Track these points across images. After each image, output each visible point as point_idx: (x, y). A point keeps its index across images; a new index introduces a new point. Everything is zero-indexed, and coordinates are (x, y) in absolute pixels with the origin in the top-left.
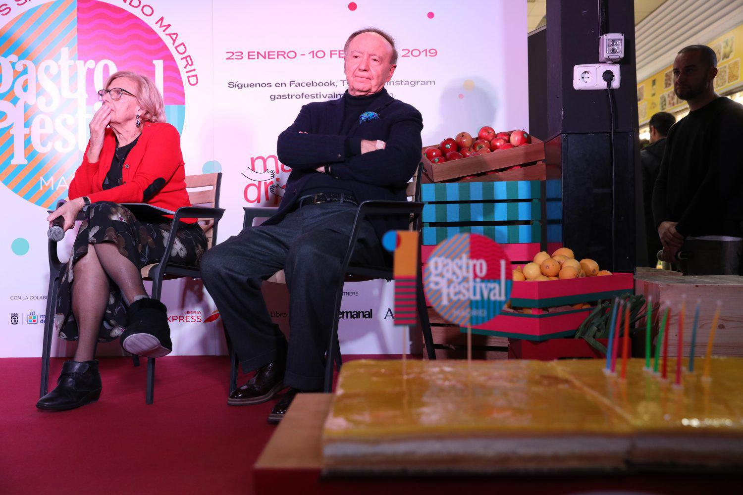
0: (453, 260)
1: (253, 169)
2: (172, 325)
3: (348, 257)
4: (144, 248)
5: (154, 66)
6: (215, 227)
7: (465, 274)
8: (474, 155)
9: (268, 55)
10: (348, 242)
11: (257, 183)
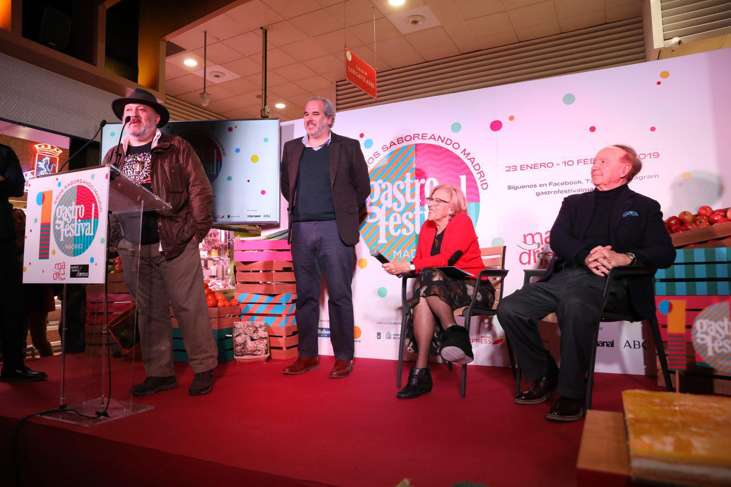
0: (716, 321)
1: (525, 243)
2: (473, 344)
3: (603, 304)
4: (455, 295)
5: (460, 179)
6: (502, 281)
7: (409, 200)
8: (696, 228)
9: (534, 167)
10: (603, 295)
11: (528, 251)
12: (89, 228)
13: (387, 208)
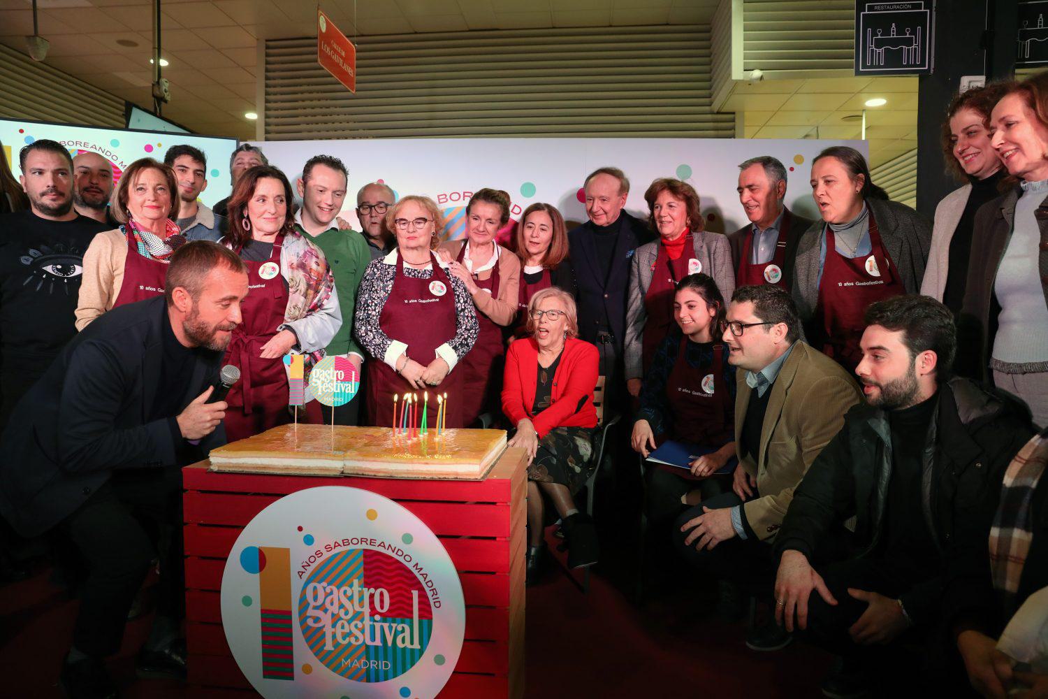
7: (358, 609)
12: (407, 634)
13: (333, 615)
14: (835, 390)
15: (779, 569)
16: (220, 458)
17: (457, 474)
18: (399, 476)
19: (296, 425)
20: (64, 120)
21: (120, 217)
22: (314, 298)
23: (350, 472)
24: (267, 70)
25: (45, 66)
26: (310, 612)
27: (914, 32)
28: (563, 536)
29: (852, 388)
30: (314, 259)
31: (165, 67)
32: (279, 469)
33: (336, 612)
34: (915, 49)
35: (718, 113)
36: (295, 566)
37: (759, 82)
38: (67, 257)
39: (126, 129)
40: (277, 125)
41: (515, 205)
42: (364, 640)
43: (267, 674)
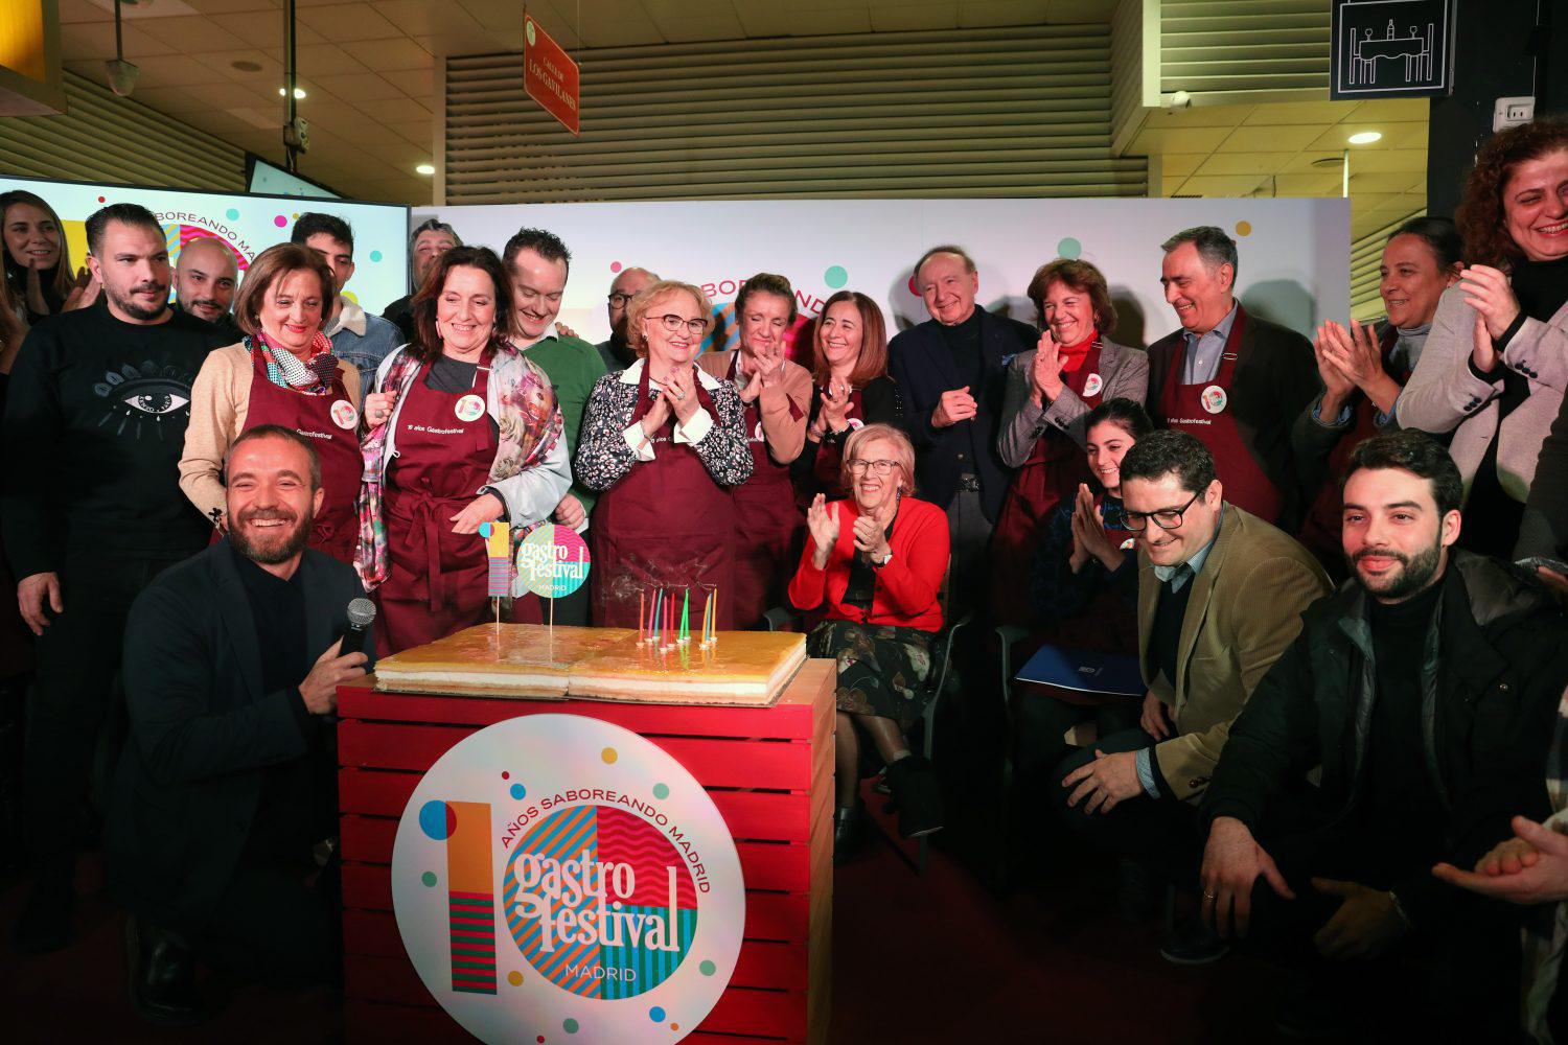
5: (667, 871)
7: (588, 892)
12: (660, 930)
13: (552, 900)
14: (1285, 577)
15: (1211, 843)
16: (390, 673)
17: (734, 697)
18: (650, 700)
19: (498, 626)
20: (164, 182)
21: (247, 327)
22: (533, 447)
23: (577, 694)
24: (449, 102)
25: (130, 102)
26: (520, 896)
27: (1422, 32)
28: (889, 791)
29: (1312, 574)
30: (536, 390)
31: (301, 100)
32: (475, 688)
33: (557, 897)
34: (1425, 57)
35: (1122, 157)
36: (498, 830)
37: (1184, 109)
38: (153, 384)
39: (247, 193)
40: (464, 183)
41: (817, 300)
42: (598, 938)
43: (459, 985)
